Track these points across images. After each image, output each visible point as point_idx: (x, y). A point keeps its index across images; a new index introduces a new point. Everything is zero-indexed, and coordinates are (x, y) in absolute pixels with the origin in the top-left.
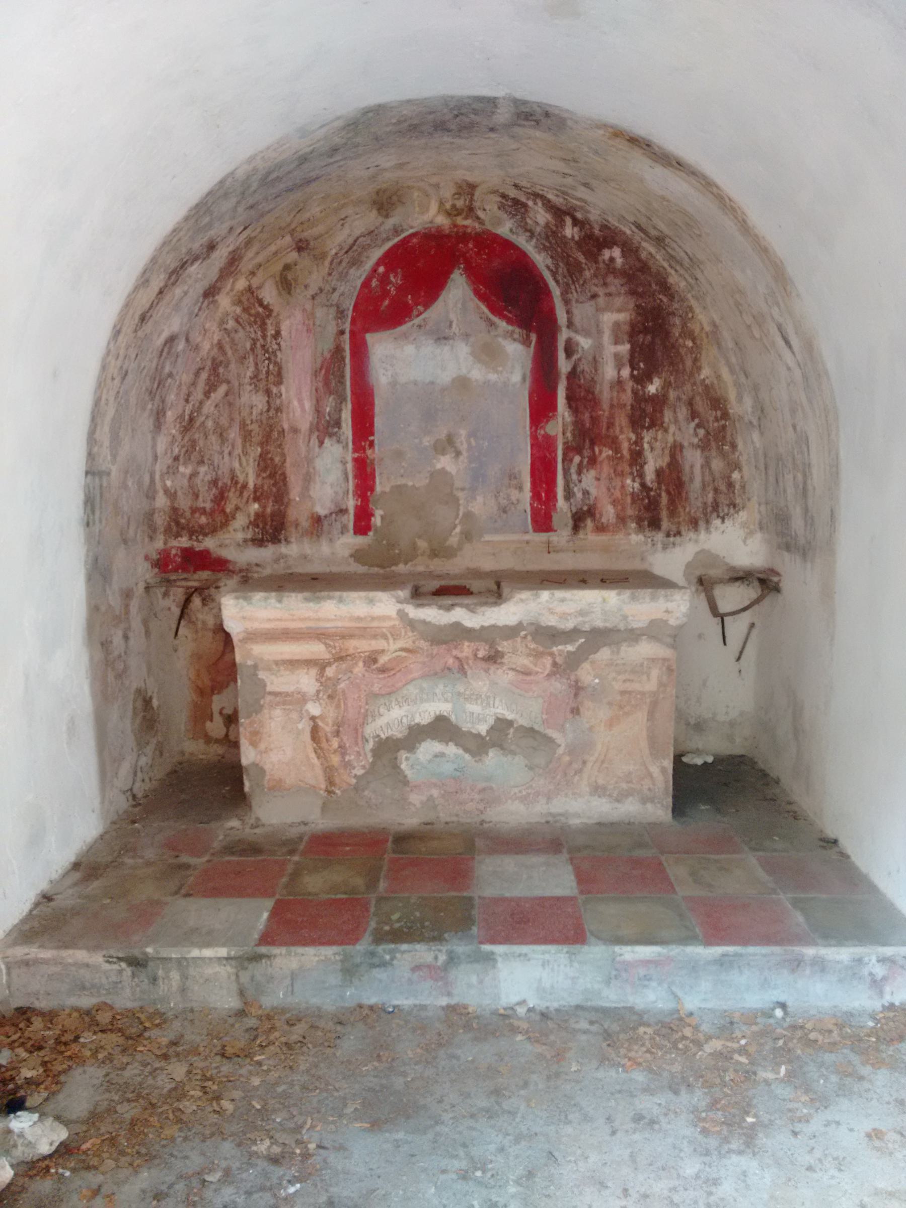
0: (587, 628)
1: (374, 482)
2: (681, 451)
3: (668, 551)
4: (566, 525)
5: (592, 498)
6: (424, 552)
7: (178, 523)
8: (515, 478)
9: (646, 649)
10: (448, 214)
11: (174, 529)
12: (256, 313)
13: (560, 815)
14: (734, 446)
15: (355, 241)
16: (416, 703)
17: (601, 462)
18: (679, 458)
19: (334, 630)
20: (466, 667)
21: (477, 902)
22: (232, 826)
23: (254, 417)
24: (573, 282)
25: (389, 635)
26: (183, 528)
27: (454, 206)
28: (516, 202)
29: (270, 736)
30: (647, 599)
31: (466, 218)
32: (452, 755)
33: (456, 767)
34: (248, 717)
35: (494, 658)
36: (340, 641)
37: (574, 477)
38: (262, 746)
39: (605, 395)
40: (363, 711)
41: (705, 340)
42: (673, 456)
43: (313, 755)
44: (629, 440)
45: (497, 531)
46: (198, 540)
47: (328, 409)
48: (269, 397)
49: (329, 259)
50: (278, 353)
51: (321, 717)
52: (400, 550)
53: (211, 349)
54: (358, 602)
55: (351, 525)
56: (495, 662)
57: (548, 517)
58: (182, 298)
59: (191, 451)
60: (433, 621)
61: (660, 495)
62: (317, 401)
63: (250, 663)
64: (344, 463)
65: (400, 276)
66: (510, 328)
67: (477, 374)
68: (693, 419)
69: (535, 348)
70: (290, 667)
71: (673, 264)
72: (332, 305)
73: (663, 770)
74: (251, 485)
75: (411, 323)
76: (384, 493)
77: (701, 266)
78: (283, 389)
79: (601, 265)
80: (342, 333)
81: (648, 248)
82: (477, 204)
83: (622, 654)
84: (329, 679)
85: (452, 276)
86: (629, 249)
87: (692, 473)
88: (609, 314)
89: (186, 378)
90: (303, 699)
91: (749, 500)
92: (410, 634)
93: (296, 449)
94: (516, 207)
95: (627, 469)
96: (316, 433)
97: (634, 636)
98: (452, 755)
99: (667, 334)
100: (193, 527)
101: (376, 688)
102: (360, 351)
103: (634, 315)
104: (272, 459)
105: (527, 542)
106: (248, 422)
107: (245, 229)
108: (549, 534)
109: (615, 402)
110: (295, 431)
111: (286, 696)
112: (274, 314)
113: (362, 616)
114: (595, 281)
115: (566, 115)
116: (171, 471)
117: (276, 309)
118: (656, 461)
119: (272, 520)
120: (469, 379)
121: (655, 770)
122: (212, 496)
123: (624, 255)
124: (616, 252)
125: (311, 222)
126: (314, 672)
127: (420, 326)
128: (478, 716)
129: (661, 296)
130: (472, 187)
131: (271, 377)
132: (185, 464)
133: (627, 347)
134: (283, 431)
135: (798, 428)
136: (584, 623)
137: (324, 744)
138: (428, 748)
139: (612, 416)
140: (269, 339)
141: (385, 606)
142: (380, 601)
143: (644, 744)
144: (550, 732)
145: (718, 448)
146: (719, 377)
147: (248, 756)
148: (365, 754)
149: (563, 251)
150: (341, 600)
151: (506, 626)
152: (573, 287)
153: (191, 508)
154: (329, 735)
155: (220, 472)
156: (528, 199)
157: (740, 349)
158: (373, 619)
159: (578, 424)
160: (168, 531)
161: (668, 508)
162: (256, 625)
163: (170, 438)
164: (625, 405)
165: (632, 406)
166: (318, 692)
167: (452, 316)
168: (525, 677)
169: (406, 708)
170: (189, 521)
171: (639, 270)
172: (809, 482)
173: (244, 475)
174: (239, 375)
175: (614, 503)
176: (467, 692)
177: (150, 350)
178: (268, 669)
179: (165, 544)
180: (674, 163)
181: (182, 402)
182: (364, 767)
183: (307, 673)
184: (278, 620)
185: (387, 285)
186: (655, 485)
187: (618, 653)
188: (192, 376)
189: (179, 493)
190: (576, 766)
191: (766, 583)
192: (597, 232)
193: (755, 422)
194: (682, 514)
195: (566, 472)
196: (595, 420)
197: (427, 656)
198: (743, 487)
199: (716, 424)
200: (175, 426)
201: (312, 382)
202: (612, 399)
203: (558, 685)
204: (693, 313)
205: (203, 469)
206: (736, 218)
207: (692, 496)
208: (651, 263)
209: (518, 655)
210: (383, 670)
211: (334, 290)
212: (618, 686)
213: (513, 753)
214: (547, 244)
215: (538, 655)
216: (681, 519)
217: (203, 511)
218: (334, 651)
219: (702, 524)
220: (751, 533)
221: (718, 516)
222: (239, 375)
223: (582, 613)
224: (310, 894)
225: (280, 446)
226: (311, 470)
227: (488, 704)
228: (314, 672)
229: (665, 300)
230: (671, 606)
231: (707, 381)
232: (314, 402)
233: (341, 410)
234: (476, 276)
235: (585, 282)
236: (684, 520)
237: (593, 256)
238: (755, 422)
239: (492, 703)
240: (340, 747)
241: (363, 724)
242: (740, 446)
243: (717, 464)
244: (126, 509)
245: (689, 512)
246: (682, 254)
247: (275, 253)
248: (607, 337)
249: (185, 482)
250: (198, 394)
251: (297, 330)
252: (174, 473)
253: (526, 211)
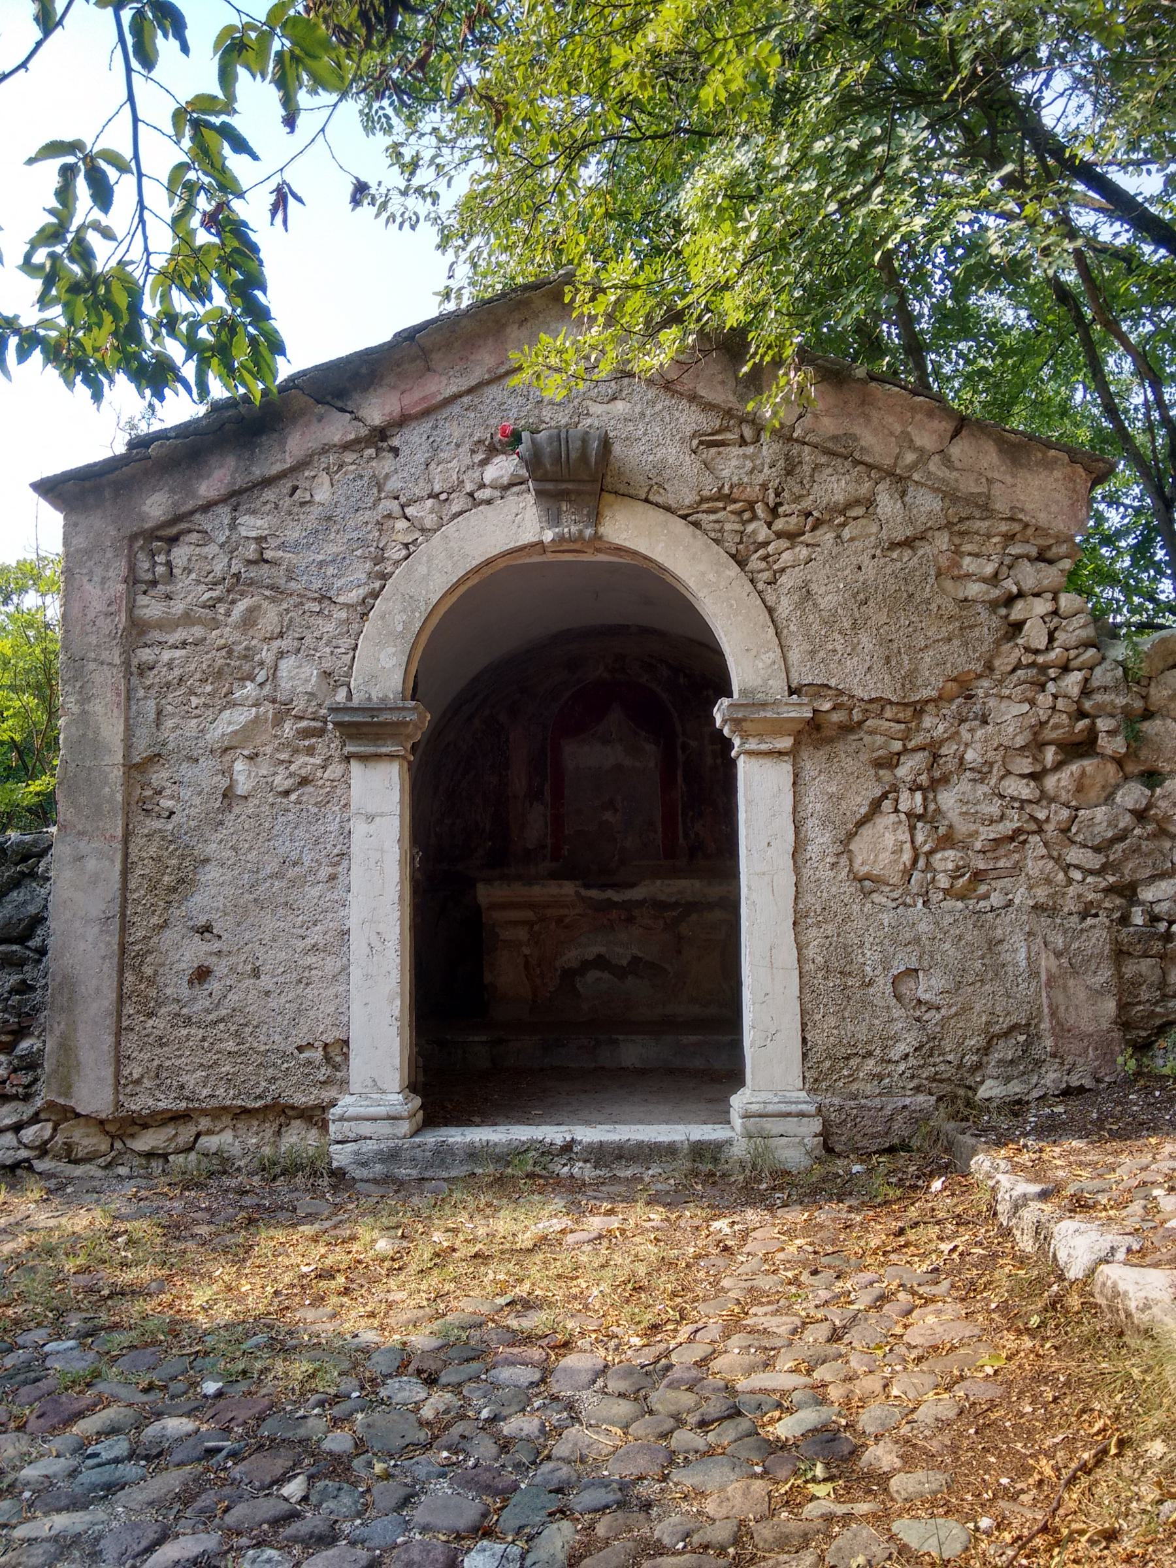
35: (630, 920)
128: (622, 956)
138: (592, 975)
141: (568, 889)
147: (488, 978)
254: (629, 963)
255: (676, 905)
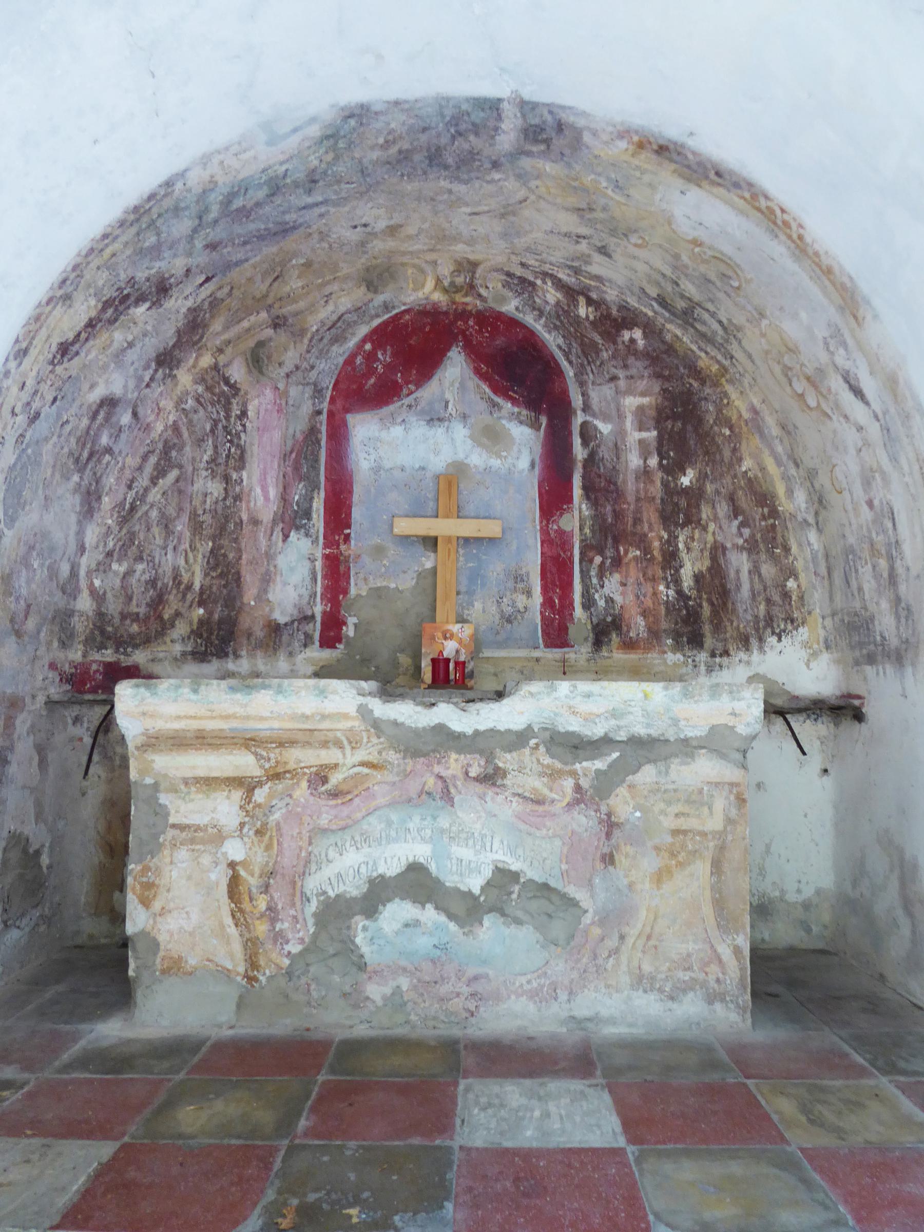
0: (622, 736)
1: (348, 583)
2: (724, 554)
3: (714, 674)
4: (586, 639)
5: (617, 608)
6: (407, 669)
7: (103, 632)
8: (522, 580)
9: (705, 769)
10: (446, 291)
11: (99, 639)
12: (222, 393)
13: (589, 1020)
14: (787, 549)
15: (340, 318)
16: (380, 844)
17: (628, 564)
18: (722, 561)
19: (268, 733)
20: (452, 790)
21: (457, 1156)
22: (110, 1030)
23: (207, 507)
24: (589, 363)
25: (345, 743)
26: (109, 638)
27: (452, 284)
28: (523, 280)
29: (168, 891)
30: (706, 697)
31: (466, 295)
32: (430, 924)
33: (436, 943)
34: (140, 861)
36: (277, 751)
37: (595, 581)
38: (157, 905)
39: (630, 486)
40: (303, 854)
41: (745, 429)
42: (714, 558)
43: (229, 921)
44: (661, 538)
45: (500, 645)
46: (125, 654)
47: (297, 498)
48: (227, 483)
49: (309, 335)
50: (243, 435)
51: (243, 863)
52: (377, 667)
53: (166, 430)
54: (303, 693)
55: (317, 636)
56: (494, 784)
57: (563, 630)
58: (124, 350)
59: (128, 546)
60: (408, 722)
61: (701, 606)
62: (285, 488)
63: (149, 781)
64: (312, 560)
65: (389, 353)
66: (516, 410)
67: (477, 459)
68: (736, 517)
69: (545, 431)
70: (205, 788)
71: (703, 345)
72: (308, 384)
73: (737, 951)
74: (197, 586)
75: (400, 403)
76: (359, 596)
77: (739, 335)
78: (245, 474)
79: (621, 347)
80: (319, 413)
81: (673, 329)
82: (478, 282)
83: (673, 775)
84: (259, 806)
85: (450, 354)
86: (650, 329)
87: (739, 579)
88: (632, 398)
89: (132, 461)
90: (219, 837)
91: (810, 613)
92: (375, 740)
93: (255, 543)
94: (523, 286)
95: (660, 573)
96: (281, 525)
97: (687, 748)
98: (430, 924)
99: (700, 421)
100: (122, 636)
101: (324, 822)
102: (338, 435)
103: (660, 400)
104: (225, 556)
105: (538, 660)
106: (200, 512)
107: (208, 280)
108: (566, 650)
109: (642, 495)
110: (255, 522)
111: (195, 831)
112: (242, 393)
113: (308, 713)
114: (614, 363)
115: (581, 122)
116: (102, 568)
117: (244, 387)
118: (693, 564)
119: (220, 629)
120: (467, 465)
121: (725, 952)
122: (148, 600)
123: (645, 336)
124: (638, 334)
125: (289, 298)
126: (238, 795)
127: (410, 406)
128: (468, 866)
129: (691, 381)
130: (474, 265)
131: (230, 461)
132: (119, 561)
133: (655, 433)
134: (241, 521)
135: (876, 502)
136: (619, 728)
137: (246, 905)
138: (397, 912)
139: (638, 511)
140: (232, 420)
141: (344, 699)
142: (335, 692)
143: (708, 910)
144: (573, 891)
145: (768, 551)
146: (763, 469)
147: (137, 920)
148: (305, 919)
149: (576, 330)
150: (280, 690)
151: (509, 731)
152: (589, 369)
153: (121, 613)
154: (254, 890)
155: (160, 571)
156: (536, 278)
157: (789, 433)
158: (324, 717)
159: (598, 518)
160: (89, 642)
161: (712, 622)
162: (160, 725)
163: (104, 530)
164: (654, 498)
165: (662, 499)
166: (242, 825)
167: (448, 396)
168: (536, 807)
169: (366, 850)
170: (116, 629)
171: (663, 353)
172: (898, 563)
173: (189, 574)
174: (194, 459)
175: (644, 614)
176: (454, 829)
177: (77, 403)
178: (174, 790)
179: (84, 656)
180: (712, 175)
181: (123, 489)
182: (302, 940)
183: (228, 798)
184: (191, 717)
185: (375, 362)
186: (694, 593)
187: (667, 773)
188: (139, 460)
189: (109, 595)
190: (612, 943)
191: (845, 710)
192: (614, 312)
193: (811, 520)
194: (729, 628)
195: (585, 575)
196: (617, 515)
197: (398, 774)
198: (801, 598)
199: (763, 523)
200: (112, 516)
201: (279, 466)
202: (638, 491)
203: (584, 820)
204: (729, 398)
205: (140, 567)
206: (790, 237)
207: (740, 608)
208: (677, 346)
209: (526, 771)
210: (335, 794)
211: (312, 367)
212: (669, 823)
213: (518, 922)
214: (558, 323)
215: (553, 775)
216: (728, 635)
217: (136, 618)
218: (267, 766)
219: (754, 642)
220: (815, 655)
221: (773, 633)
222: (194, 459)
223: (614, 714)
224: (180, 1136)
225: (236, 540)
226: (272, 569)
227: (484, 846)
228: (238, 795)
229: (695, 384)
230: (739, 706)
231: (749, 474)
232: (281, 489)
233: (312, 498)
234: (474, 352)
235: (602, 363)
236: (732, 637)
237: (611, 336)
238: (811, 520)
239: (488, 844)
240: (269, 908)
241: (304, 874)
242: (794, 549)
243: (768, 570)
244: (24, 592)
245: (738, 628)
246: (715, 326)
247: (248, 330)
248: (629, 423)
249: (118, 582)
250: (143, 481)
251: (266, 410)
252: (105, 572)
253: (534, 289)
254: (488, 885)
255: (606, 742)
